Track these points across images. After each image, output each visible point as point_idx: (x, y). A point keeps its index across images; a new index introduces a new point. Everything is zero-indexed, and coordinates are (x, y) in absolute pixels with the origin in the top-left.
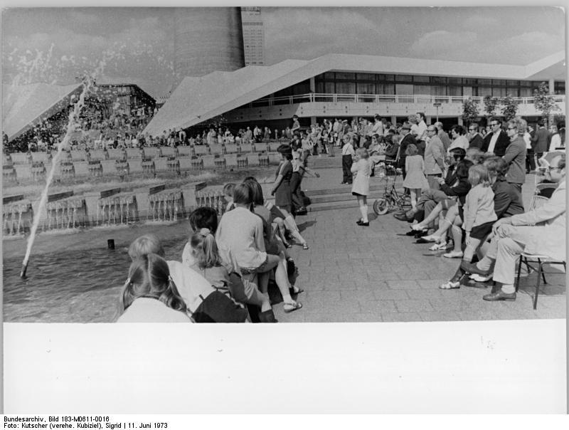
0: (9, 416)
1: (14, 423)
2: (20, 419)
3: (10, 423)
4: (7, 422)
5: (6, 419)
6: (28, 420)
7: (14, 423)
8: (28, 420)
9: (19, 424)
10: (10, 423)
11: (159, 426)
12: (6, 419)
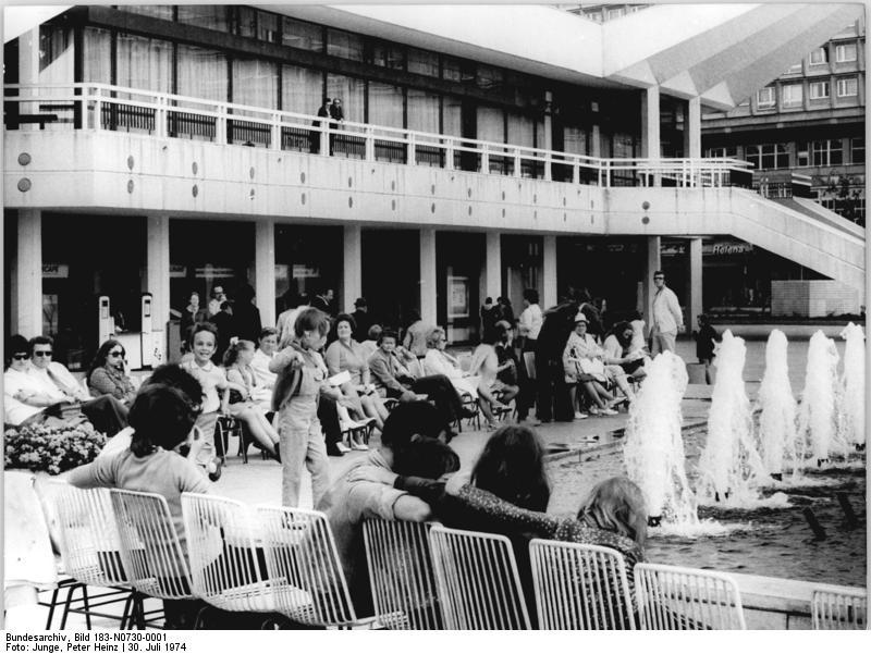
0: (14, 634)
1: (21, 643)
2: (30, 638)
3: (15, 643)
4: (11, 641)
5: (8, 637)
7: (21, 643)
9: (32, 644)
11: (172, 649)
12: (8, 637)
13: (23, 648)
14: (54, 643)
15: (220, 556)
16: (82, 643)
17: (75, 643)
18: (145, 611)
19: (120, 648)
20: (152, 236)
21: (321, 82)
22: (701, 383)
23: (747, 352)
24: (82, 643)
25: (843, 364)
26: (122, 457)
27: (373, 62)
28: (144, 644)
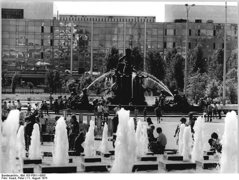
0: (4, 174)
1: (6, 177)
2: (8, 176)
3: (4, 177)
5: (2, 175)
6: (12, 176)
7: (6, 177)
8: (12, 176)
9: (8, 177)
10: (4, 177)
13: (6, 178)
14: (15, 177)
15: (181, 158)
16: (22, 177)
17: (20, 177)
18: (166, 149)
19: (25, 178)
20: (54, 164)
21: (158, 33)
22: (23, 167)
23: (166, 145)
24: (22, 177)
25: (26, 145)
26: (46, 164)
27: (133, 71)
28: (31, 177)
